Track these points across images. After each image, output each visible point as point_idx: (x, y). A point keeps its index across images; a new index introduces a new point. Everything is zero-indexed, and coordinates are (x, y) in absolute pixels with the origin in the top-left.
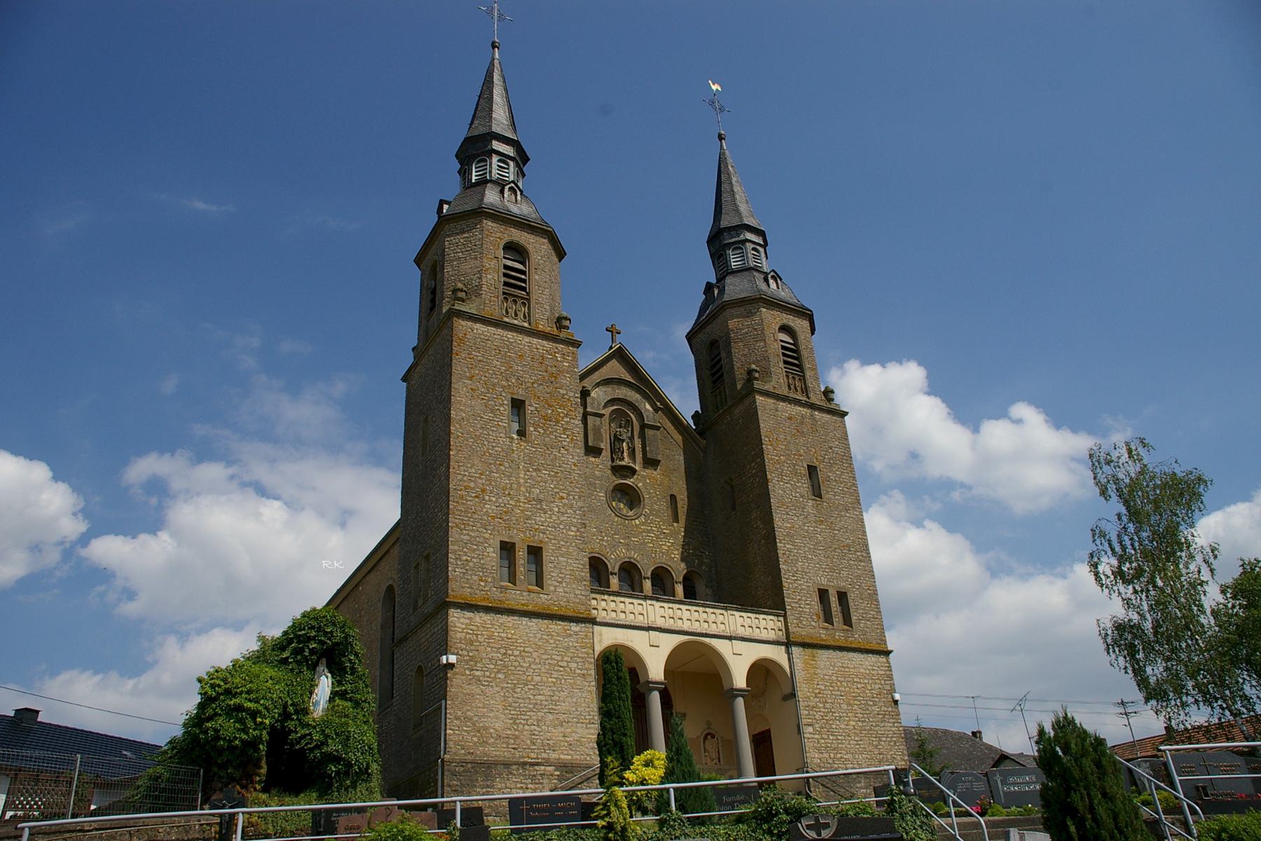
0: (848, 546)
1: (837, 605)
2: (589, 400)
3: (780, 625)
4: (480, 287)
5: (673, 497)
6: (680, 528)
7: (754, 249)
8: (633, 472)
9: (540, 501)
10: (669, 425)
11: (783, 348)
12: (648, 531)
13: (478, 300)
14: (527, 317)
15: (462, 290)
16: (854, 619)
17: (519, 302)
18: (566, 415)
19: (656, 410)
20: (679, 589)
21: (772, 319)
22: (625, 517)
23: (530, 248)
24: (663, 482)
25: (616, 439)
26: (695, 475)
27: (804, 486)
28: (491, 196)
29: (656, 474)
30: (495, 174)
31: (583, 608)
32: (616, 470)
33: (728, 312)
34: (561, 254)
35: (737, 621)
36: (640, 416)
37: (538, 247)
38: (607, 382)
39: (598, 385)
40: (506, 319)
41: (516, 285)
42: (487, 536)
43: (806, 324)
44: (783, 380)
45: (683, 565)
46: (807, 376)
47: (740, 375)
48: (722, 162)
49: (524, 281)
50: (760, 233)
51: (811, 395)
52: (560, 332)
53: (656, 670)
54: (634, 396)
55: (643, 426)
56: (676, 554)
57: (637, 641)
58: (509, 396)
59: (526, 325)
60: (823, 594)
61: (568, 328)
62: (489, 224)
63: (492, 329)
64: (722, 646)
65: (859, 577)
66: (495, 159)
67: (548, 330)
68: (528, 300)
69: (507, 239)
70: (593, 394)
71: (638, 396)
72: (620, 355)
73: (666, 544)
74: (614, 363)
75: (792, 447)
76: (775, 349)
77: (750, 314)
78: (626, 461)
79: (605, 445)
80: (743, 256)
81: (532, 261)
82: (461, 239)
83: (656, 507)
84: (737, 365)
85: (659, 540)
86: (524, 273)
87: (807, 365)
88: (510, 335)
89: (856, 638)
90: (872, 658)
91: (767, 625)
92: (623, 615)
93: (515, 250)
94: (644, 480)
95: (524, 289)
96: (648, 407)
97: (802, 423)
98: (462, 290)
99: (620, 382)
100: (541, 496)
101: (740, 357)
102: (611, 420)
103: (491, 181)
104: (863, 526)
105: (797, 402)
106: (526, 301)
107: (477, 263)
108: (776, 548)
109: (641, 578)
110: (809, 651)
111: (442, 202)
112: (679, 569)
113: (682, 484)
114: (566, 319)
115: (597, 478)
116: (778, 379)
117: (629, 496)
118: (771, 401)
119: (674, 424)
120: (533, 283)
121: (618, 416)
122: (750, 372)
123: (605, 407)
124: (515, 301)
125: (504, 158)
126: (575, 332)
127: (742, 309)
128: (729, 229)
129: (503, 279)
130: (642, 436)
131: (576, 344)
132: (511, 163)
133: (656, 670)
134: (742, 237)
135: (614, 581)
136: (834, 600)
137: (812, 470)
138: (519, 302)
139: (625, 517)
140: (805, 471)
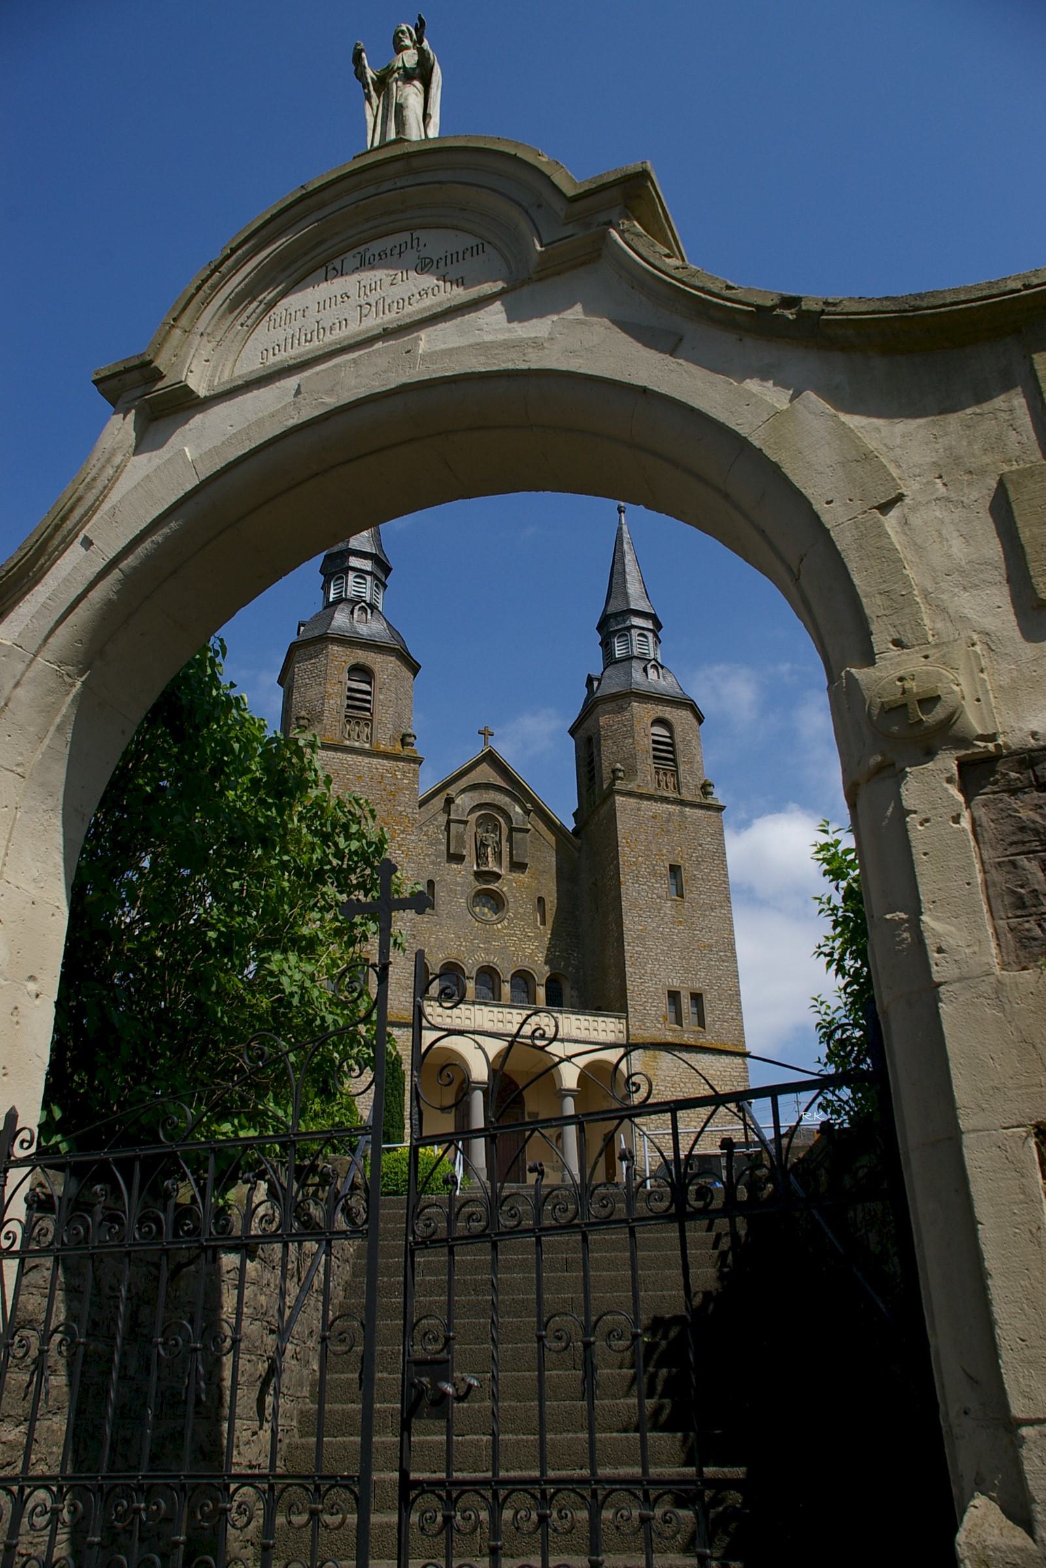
0: (710, 946)
1: (688, 1004)
2: (453, 807)
3: (622, 1027)
4: (322, 712)
5: (541, 900)
6: (547, 931)
7: (640, 635)
8: (497, 876)
10: (542, 827)
11: (654, 742)
13: (319, 726)
14: (369, 739)
15: (303, 718)
16: (708, 1020)
17: (362, 723)
18: (403, 832)
19: (527, 812)
20: (541, 992)
21: (643, 713)
22: (486, 922)
23: (376, 668)
24: (532, 885)
25: (481, 846)
26: (567, 876)
27: (663, 886)
28: (341, 619)
29: (524, 877)
30: (351, 593)
32: (479, 875)
33: (600, 708)
34: (414, 668)
35: (573, 1024)
36: (509, 819)
37: (385, 666)
39: (463, 791)
40: (347, 743)
41: (358, 708)
43: (687, 715)
44: (650, 777)
45: (547, 968)
46: (681, 771)
47: (606, 773)
49: (368, 702)
50: (652, 617)
51: (682, 791)
52: (405, 751)
53: (479, 1071)
54: (502, 799)
55: (512, 830)
56: (541, 958)
57: (461, 1045)
59: (367, 746)
60: (674, 996)
61: (412, 745)
62: (334, 649)
65: (719, 978)
66: (351, 575)
67: (389, 749)
68: (371, 720)
69: (352, 661)
70: (457, 801)
71: (507, 799)
72: (490, 758)
73: (529, 947)
74: (484, 766)
75: (653, 847)
76: (645, 744)
77: (621, 710)
78: (492, 866)
79: (469, 851)
80: (628, 644)
81: (377, 680)
82: (307, 665)
83: (521, 910)
84: (605, 764)
85: (524, 943)
86: (369, 693)
87: (681, 759)
88: (350, 758)
89: (707, 1040)
91: (606, 1028)
92: (449, 1020)
93: (361, 672)
94: (510, 884)
95: (368, 710)
96: (518, 809)
97: (669, 821)
98: (303, 718)
99: (488, 786)
101: (608, 756)
102: (478, 825)
103: (346, 600)
104: (731, 925)
105: (665, 800)
106: (369, 722)
107: (321, 689)
109: (535, 985)
110: (650, 1053)
111: (301, 624)
112: (542, 972)
113: (553, 886)
114: (410, 735)
115: (457, 884)
116: (646, 776)
117: (496, 901)
118: (633, 801)
119: (549, 828)
120: (376, 703)
121: (488, 822)
122: (614, 771)
123: (472, 811)
124: (358, 723)
125: (361, 573)
126: (419, 749)
127: (614, 704)
128: (615, 615)
129: (346, 702)
130: (510, 839)
131: (418, 761)
132: (369, 578)
133: (479, 1071)
134: (628, 623)
135: (506, 988)
136: (686, 1002)
137: (675, 870)
138: (362, 723)
139: (486, 922)
140: (665, 871)
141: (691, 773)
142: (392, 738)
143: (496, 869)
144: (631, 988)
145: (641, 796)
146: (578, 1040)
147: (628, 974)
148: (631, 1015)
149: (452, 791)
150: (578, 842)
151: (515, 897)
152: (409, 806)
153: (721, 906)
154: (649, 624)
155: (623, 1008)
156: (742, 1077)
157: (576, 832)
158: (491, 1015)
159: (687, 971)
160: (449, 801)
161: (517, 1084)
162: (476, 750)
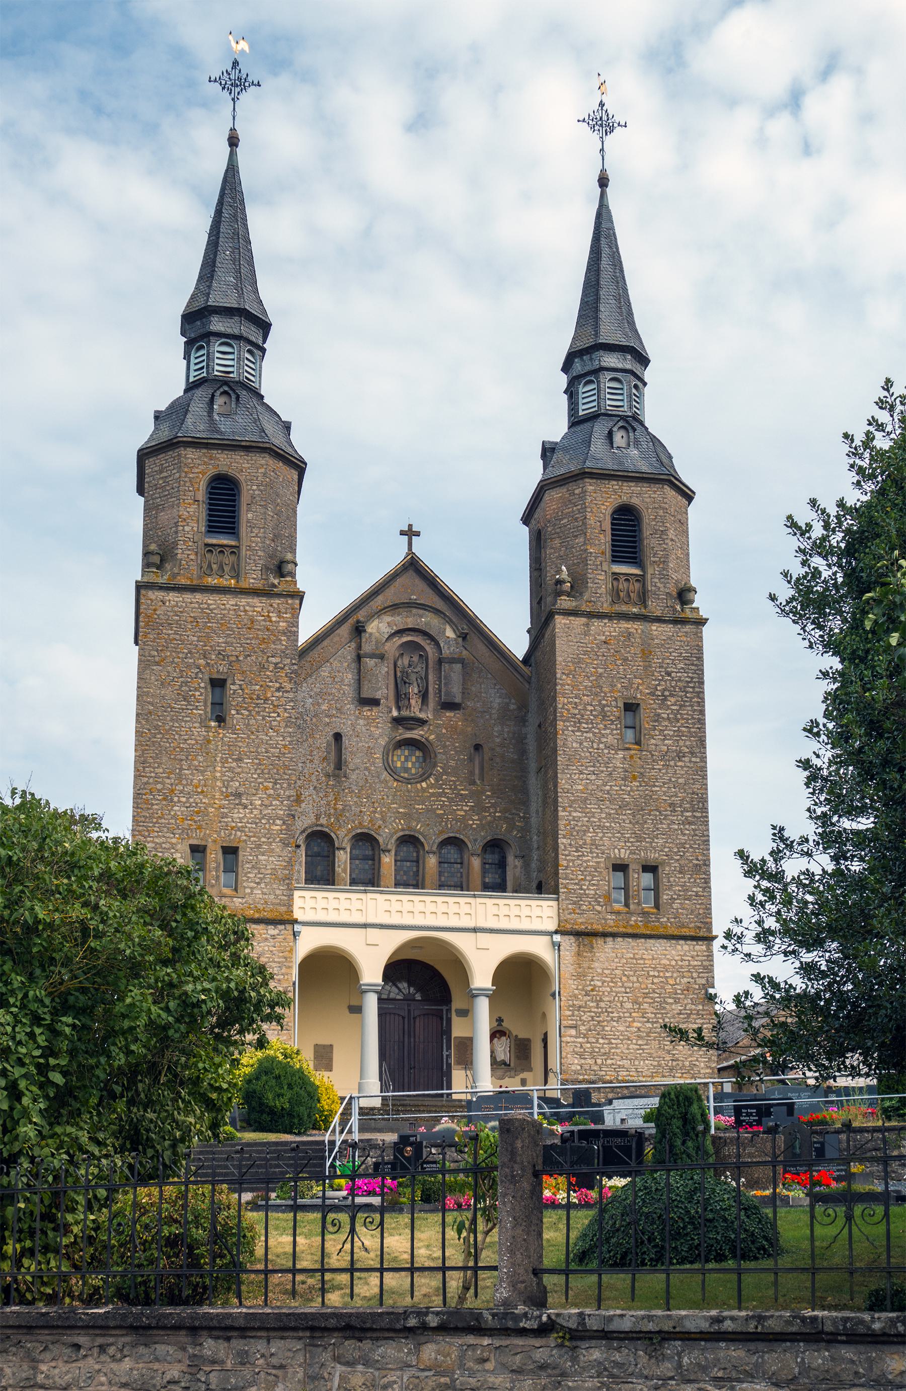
4: (176, 544)
8: (422, 722)
9: (238, 795)
12: (440, 795)
18: (278, 690)
31: (283, 909)
38: (394, 608)
42: (174, 841)
48: (603, 217)
54: (426, 620)
57: (347, 941)
58: (207, 677)
63: (188, 597)
64: (462, 943)
65: (683, 845)
78: (415, 709)
79: (383, 690)
90: (684, 947)
100: (242, 789)
108: (556, 817)
137: (631, 707)
138: (227, 551)
140: (615, 710)
141: (664, 577)
142: (266, 569)
143: (422, 716)
144: (565, 863)
145: (591, 615)
146: (487, 930)
147: (562, 847)
148: (562, 896)
149: (361, 615)
150: (526, 670)
151: (444, 747)
152: (286, 656)
153: (692, 753)
154: (628, 363)
155: (556, 891)
156: (705, 967)
157: (526, 660)
158: (386, 906)
159: (639, 839)
160: (359, 630)
161: (424, 980)
162: (396, 557)
